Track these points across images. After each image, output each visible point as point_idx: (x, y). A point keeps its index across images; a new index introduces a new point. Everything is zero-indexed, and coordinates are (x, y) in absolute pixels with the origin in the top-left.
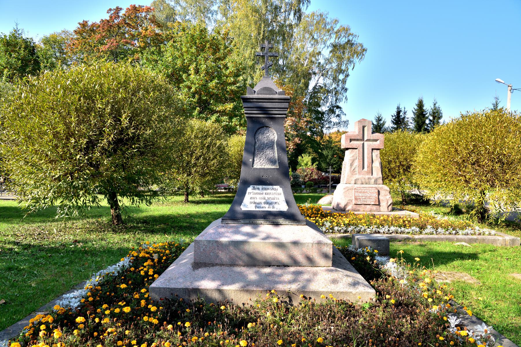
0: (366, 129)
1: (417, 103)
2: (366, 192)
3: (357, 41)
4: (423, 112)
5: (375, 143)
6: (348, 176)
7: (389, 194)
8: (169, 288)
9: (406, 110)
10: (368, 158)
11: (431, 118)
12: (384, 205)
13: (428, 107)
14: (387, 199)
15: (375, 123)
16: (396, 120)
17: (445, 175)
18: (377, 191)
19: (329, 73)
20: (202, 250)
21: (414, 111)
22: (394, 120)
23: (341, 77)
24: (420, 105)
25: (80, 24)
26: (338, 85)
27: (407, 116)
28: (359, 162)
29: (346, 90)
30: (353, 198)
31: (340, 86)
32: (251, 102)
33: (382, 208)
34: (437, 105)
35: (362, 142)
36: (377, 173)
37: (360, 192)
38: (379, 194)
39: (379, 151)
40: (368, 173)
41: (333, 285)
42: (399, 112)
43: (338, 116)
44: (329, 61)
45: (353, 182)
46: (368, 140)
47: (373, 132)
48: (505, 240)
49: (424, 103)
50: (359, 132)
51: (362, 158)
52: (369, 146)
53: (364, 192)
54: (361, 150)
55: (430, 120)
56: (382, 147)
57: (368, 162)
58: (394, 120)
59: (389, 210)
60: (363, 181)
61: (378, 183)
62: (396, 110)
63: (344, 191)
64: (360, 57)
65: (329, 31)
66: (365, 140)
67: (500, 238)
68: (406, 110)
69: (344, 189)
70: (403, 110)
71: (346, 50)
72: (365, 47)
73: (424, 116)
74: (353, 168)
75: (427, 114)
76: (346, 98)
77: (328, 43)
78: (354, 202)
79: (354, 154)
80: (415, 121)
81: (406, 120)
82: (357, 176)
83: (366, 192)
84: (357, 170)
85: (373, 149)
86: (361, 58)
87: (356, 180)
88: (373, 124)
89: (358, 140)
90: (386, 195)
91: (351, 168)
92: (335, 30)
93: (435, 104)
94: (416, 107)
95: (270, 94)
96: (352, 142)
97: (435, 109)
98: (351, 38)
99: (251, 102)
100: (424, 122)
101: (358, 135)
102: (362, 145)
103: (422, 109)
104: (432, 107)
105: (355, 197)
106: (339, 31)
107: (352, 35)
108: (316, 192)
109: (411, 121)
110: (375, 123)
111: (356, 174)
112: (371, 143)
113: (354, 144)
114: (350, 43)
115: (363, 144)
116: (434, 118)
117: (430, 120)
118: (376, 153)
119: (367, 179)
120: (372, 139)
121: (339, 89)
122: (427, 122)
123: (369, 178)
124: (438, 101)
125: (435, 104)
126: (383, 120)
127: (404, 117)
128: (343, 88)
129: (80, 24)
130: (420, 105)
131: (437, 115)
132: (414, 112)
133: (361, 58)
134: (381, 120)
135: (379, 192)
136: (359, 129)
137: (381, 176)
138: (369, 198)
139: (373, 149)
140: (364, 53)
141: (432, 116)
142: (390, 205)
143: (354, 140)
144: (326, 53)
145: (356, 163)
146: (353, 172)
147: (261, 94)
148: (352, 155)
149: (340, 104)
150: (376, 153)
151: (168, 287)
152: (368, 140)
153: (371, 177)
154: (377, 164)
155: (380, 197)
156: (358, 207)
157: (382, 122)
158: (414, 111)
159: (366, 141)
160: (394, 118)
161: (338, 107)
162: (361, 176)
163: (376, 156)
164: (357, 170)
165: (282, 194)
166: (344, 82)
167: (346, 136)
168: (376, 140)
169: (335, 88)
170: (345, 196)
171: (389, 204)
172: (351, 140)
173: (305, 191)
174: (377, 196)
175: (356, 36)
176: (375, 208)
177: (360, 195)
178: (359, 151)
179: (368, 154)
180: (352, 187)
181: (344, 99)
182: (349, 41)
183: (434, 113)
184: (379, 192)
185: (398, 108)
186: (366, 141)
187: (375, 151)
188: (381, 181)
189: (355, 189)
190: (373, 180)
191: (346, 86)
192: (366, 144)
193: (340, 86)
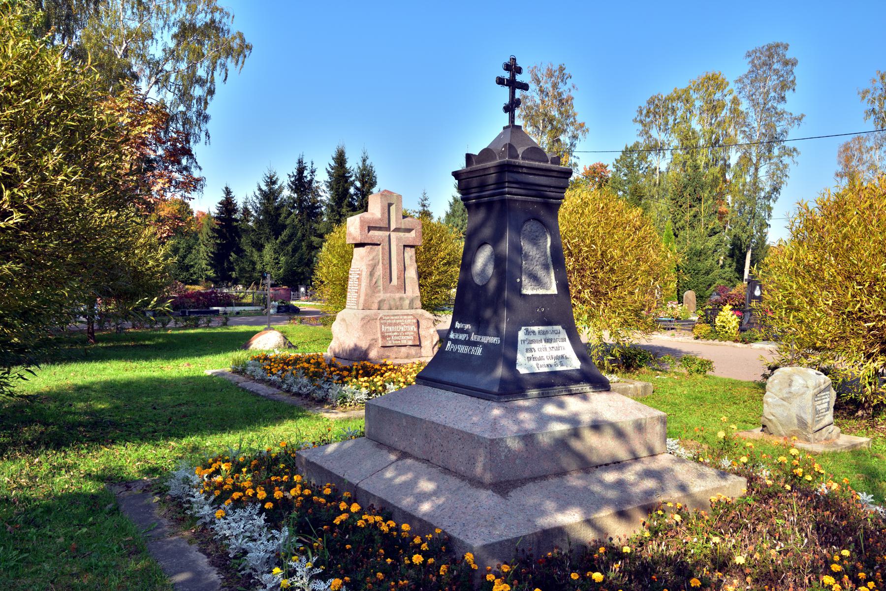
0: (393, 208)
1: (334, 156)
2: (399, 324)
4: (344, 174)
5: (407, 235)
6: (366, 295)
8: (508, 540)
9: (314, 166)
10: (398, 262)
11: (358, 184)
13: (353, 164)
15: (264, 188)
16: (296, 185)
18: (415, 321)
19: (172, 79)
20: (503, 458)
21: (330, 169)
22: (292, 183)
23: (198, 91)
24: (340, 159)
27: (316, 178)
28: (384, 268)
29: (206, 118)
30: (379, 335)
32: (519, 173)
34: (368, 162)
35: (387, 233)
36: (413, 290)
37: (390, 325)
39: (413, 249)
41: (699, 481)
42: (301, 170)
43: (186, 168)
44: (172, 54)
45: (376, 306)
48: (636, 388)
49: (347, 156)
50: (383, 214)
52: (399, 239)
53: (396, 324)
54: (387, 248)
55: (357, 188)
56: (419, 242)
57: (398, 268)
58: (292, 183)
60: (392, 303)
61: (415, 306)
62: (296, 166)
63: (362, 323)
67: (632, 386)
68: (314, 166)
69: (363, 319)
70: (309, 165)
73: (346, 179)
74: (374, 280)
75: (351, 176)
77: (174, 18)
78: (380, 343)
79: (374, 254)
80: (332, 189)
81: (314, 185)
82: (381, 295)
83: (399, 324)
84: (380, 283)
85: (405, 246)
87: (380, 302)
88: (260, 189)
90: (428, 328)
91: (371, 280)
93: (364, 161)
94: (333, 163)
95: (540, 161)
96: (372, 232)
97: (365, 169)
99: (519, 173)
100: (347, 190)
101: (381, 220)
102: (387, 239)
103: (344, 167)
104: (361, 165)
105: (382, 333)
107: (222, 10)
108: (197, 326)
109: (324, 187)
110: (264, 188)
112: (402, 234)
116: (363, 184)
117: (357, 188)
118: (410, 253)
119: (397, 300)
121: (192, 114)
122: (352, 190)
124: (369, 154)
125: (364, 161)
126: (279, 183)
127: (311, 182)
130: (340, 159)
131: (368, 179)
132: (328, 172)
134: (274, 183)
135: (418, 322)
136: (383, 209)
140: (247, 53)
141: (360, 181)
147: (528, 159)
150: (410, 254)
151: (504, 538)
153: (404, 295)
154: (412, 273)
156: (387, 352)
157: (276, 187)
158: (330, 169)
160: (293, 179)
162: (388, 295)
164: (380, 283)
165: (567, 339)
167: (362, 222)
168: (409, 230)
170: (365, 333)
171: (434, 343)
172: (370, 229)
173: (171, 324)
174: (416, 330)
175: (228, 14)
176: (413, 351)
177: (390, 329)
178: (383, 249)
179: (398, 255)
180: (375, 315)
181: (203, 135)
182: (213, 21)
183: (363, 176)
184: (418, 322)
185: (300, 162)
187: (408, 249)
188: (418, 304)
190: (407, 302)
191: (208, 112)
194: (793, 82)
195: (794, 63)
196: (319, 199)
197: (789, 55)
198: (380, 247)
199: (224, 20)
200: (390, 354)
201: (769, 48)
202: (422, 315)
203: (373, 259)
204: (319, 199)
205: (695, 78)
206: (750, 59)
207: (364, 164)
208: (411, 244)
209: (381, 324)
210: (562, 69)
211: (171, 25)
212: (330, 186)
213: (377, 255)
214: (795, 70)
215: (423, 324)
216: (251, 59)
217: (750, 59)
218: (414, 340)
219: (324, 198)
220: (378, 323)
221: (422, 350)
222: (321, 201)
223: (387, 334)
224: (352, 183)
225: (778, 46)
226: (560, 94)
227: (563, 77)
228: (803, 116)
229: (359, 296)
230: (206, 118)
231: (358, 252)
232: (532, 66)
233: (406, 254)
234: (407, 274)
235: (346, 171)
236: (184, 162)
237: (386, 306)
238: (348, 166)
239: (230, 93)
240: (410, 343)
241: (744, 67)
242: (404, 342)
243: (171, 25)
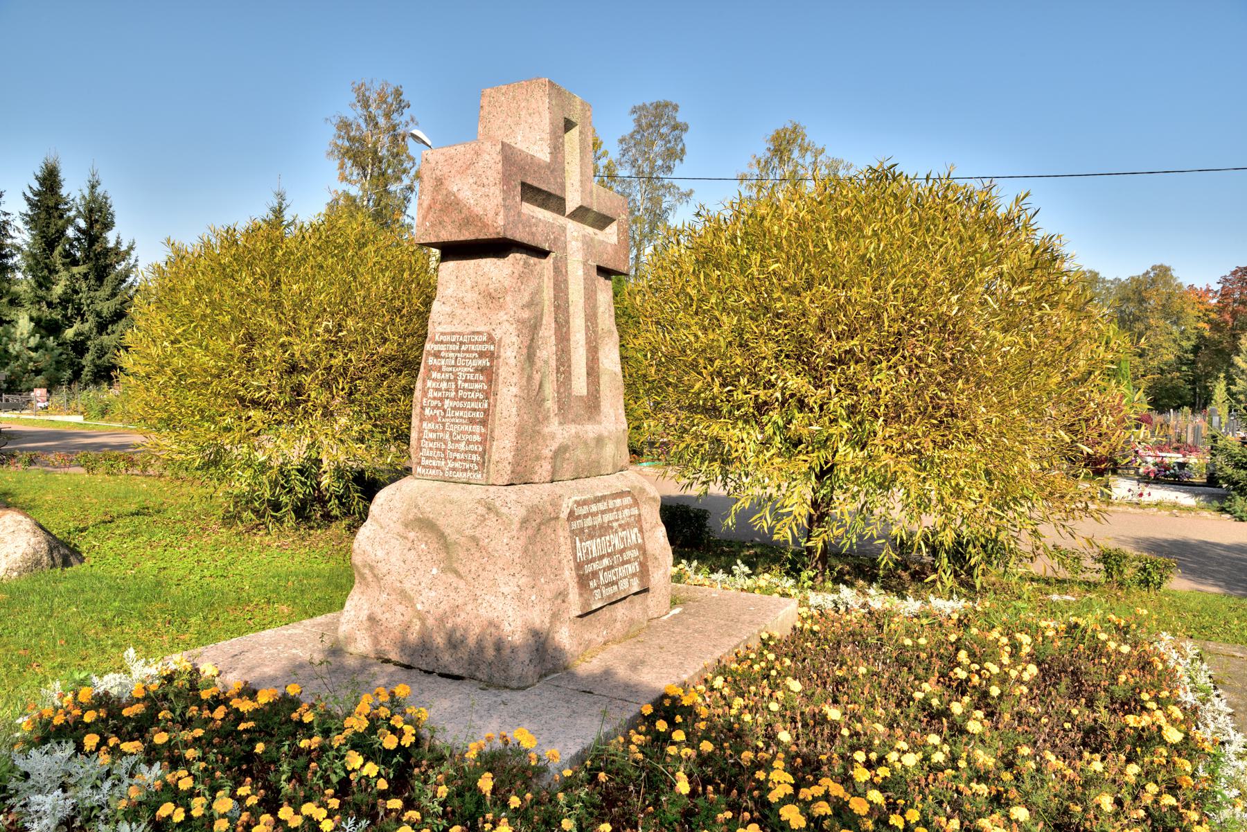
4: (57, 204)
11: (82, 224)
13: (73, 189)
21: (31, 196)
24: (50, 180)
30: (569, 575)
34: (99, 190)
45: (544, 470)
49: (62, 176)
55: (79, 230)
75: (69, 210)
93: (93, 187)
94: (36, 186)
104: (86, 192)
109: (19, 223)
116: (91, 224)
122: (70, 232)
124: (102, 177)
125: (93, 187)
130: (50, 180)
132: (28, 199)
158: (31, 196)
183: (91, 211)
194: (683, 150)
195: (684, 128)
196: (9, 241)
197: (680, 118)
198: (547, 263)
201: (657, 106)
204: (9, 241)
205: (190, 240)
206: (635, 116)
207: (92, 193)
210: (398, 93)
212: (32, 221)
213: (538, 291)
214: (684, 136)
217: (635, 116)
219: (18, 242)
220: (563, 535)
222: (13, 245)
223: (588, 569)
224: (70, 221)
225: (666, 105)
226: (394, 128)
227: (401, 106)
228: (691, 191)
229: (486, 440)
231: (455, 279)
232: (358, 82)
235: (59, 200)
237: (567, 469)
238: (63, 192)
241: (629, 126)
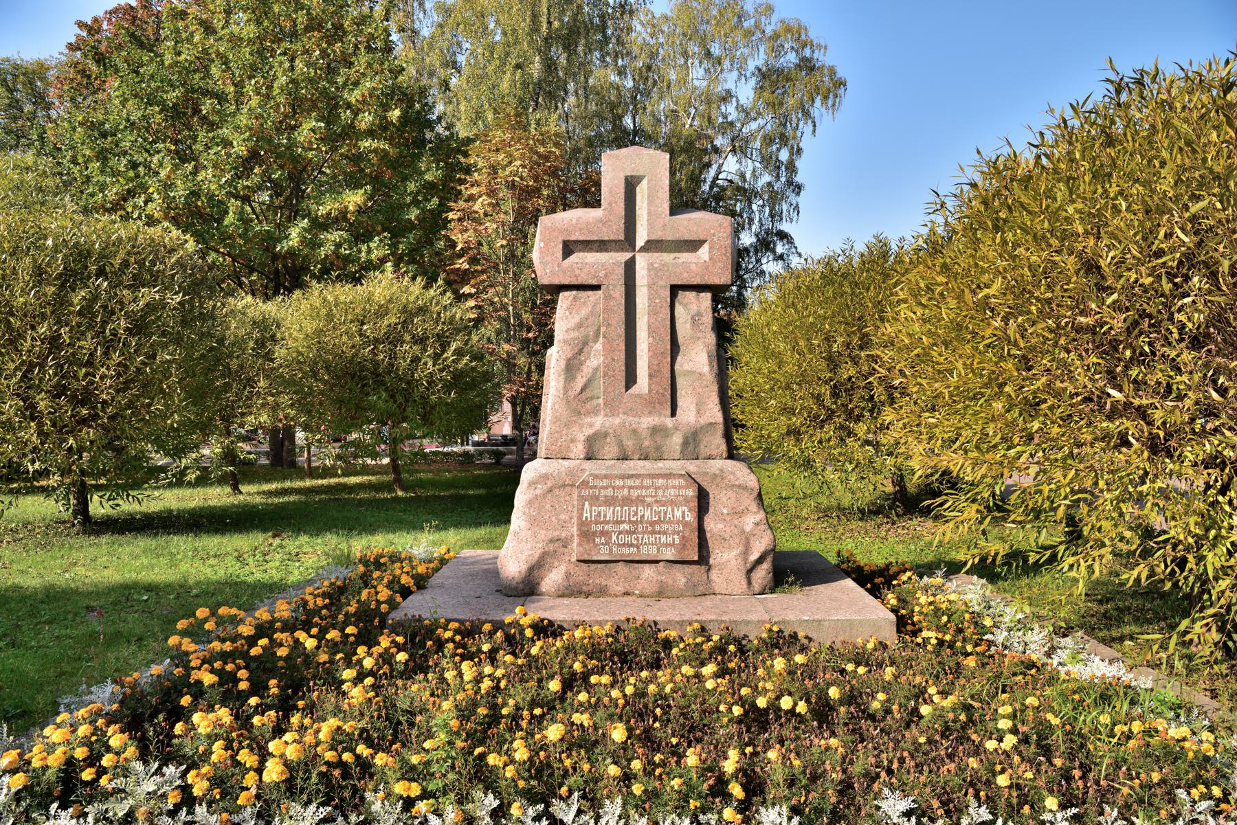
0: (642, 191)
2: (640, 500)
3: (824, 59)
5: (685, 257)
7: (754, 507)
10: (651, 331)
12: (726, 558)
14: (740, 532)
17: (1032, 407)
18: (691, 492)
25: (81, 24)
26: (778, 177)
28: (609, 350)
29: (798, 188)
31: (783, 179)
33: (718, 579)
37: (610, 502)
38: (703, 501)
40: (650, 404)
43: (781, 257)
45: (579, 449)
46: (653, 245)
47: (674, 211)
51: (621, 330)
52: (651, 268)
53: (627, 501)
54: (619, 293)
59: (757, 587)
60: (629, 443)
61: (703, 451)
64: (830, 102)
65: (749, 33)
66: (640, 243)
71: (799, 82)
72: (841, 73)
74: (580, 382)
76: (797, 208)
77: (751, 66)
78: (576, 549)
79: (584, 312)
82: (599, 422)
83: (640, 500)
84: (599, 386)
85: (675, 289)
86: (834, 105)
87: (591, 441)
89: (602, 245)
92: (769, 31)
96: (576, 258)
98: (807, 52)
102: (621, 271)
105: (582, 524)
106: (776, 36)
111: (595, 412)
112: (667, 257)
113: (587, 264)
114: (807, 65)
115: (630, 266)
119: (645, 433)
120: (670, 236)
123: (655, 431)
128: (790, 183)
129: (81, 24)
133: (834, 105)
137: (719, 417)
138: (653, 528)
139: (675, 289)
142: (760, 561)
143: (587, 245)
144: (746, 92)
145: (595, 359)
146: (579, 403)
148: (576, 319)
149: (785, 226)
150: (694, 308)
152: (652, 246)
153: (669, 422)
155: (710, 524)
156: (598, 577)
159: (643, 249)
161: (783, 236)
162: (617, 421)
163: (695, 319)
166: (791, 167)
168: (693, 245)
169: (769, 184)
171: (754, 557)
174: (691, 517)
175: (819, 46)
176: (680, 577)
178: (608, 298)
179: (653, 312)
180: (570, 473)
186: (643, 249)
189: (585, 484)
190: (677, 440)
191: (799, 179)
192: (642, 262)
193: (783, 179)
199: (816, 56)
200: (610, 582)
202: (720, 476)
203: (579, 326)
208: (696, 281)
209: (582, 499)
211: (748, 74)
215: (721, 502)
216: (850, 99)
218: (683, 546)
221: (714, 574)
230: (798, 188)
233: (679, 309)
234: (682, 364)
236: (780, 249)
237: (610, 449)
239: (821, 147)
240: (670, 554)
242: (650, 552)
243: (748, 74)
